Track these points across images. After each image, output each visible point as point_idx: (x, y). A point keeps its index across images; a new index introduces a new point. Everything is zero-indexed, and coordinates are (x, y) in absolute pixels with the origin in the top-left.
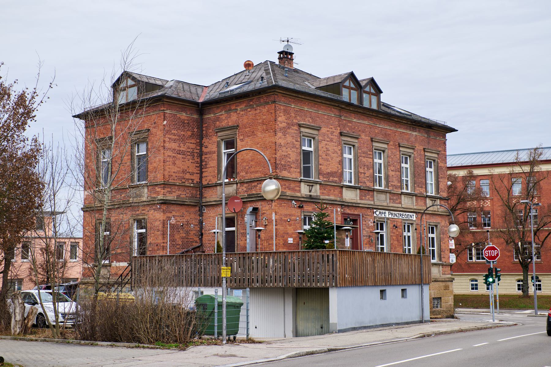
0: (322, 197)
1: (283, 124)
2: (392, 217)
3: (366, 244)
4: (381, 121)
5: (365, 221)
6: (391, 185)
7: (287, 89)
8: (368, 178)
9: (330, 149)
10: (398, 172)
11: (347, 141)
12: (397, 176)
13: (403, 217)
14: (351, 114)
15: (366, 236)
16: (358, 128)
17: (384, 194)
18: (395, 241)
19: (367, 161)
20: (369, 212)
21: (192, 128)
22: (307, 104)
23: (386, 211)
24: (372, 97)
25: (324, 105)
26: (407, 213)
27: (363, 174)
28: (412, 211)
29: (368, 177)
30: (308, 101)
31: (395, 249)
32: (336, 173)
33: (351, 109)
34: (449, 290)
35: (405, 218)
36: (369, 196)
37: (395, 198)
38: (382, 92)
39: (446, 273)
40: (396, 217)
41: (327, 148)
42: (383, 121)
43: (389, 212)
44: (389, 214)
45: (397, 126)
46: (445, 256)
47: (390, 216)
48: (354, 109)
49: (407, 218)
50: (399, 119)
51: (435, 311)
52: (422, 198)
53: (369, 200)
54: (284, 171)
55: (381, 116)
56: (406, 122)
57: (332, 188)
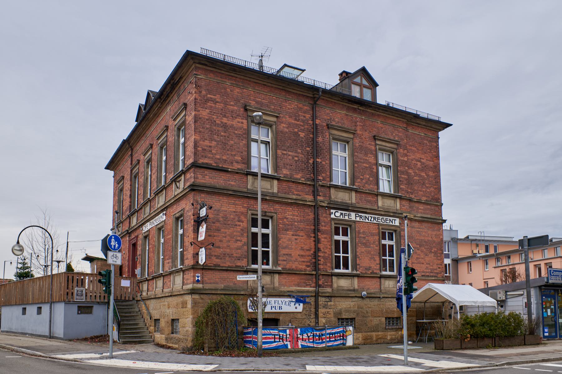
0: (357, 205)
2: (361, 220)
7: (309, 88)
13: (379, 221)
17: (348, 193)
21: (303, 146)
24: (365, 90)
26: (385, 218)
35: (381, 223)
38: (378, 85)
40: (367, 221)
43: (356, 214)
44: (356, 217)
47: (358, 219)
49: (385, 223)
51: (171, 339)
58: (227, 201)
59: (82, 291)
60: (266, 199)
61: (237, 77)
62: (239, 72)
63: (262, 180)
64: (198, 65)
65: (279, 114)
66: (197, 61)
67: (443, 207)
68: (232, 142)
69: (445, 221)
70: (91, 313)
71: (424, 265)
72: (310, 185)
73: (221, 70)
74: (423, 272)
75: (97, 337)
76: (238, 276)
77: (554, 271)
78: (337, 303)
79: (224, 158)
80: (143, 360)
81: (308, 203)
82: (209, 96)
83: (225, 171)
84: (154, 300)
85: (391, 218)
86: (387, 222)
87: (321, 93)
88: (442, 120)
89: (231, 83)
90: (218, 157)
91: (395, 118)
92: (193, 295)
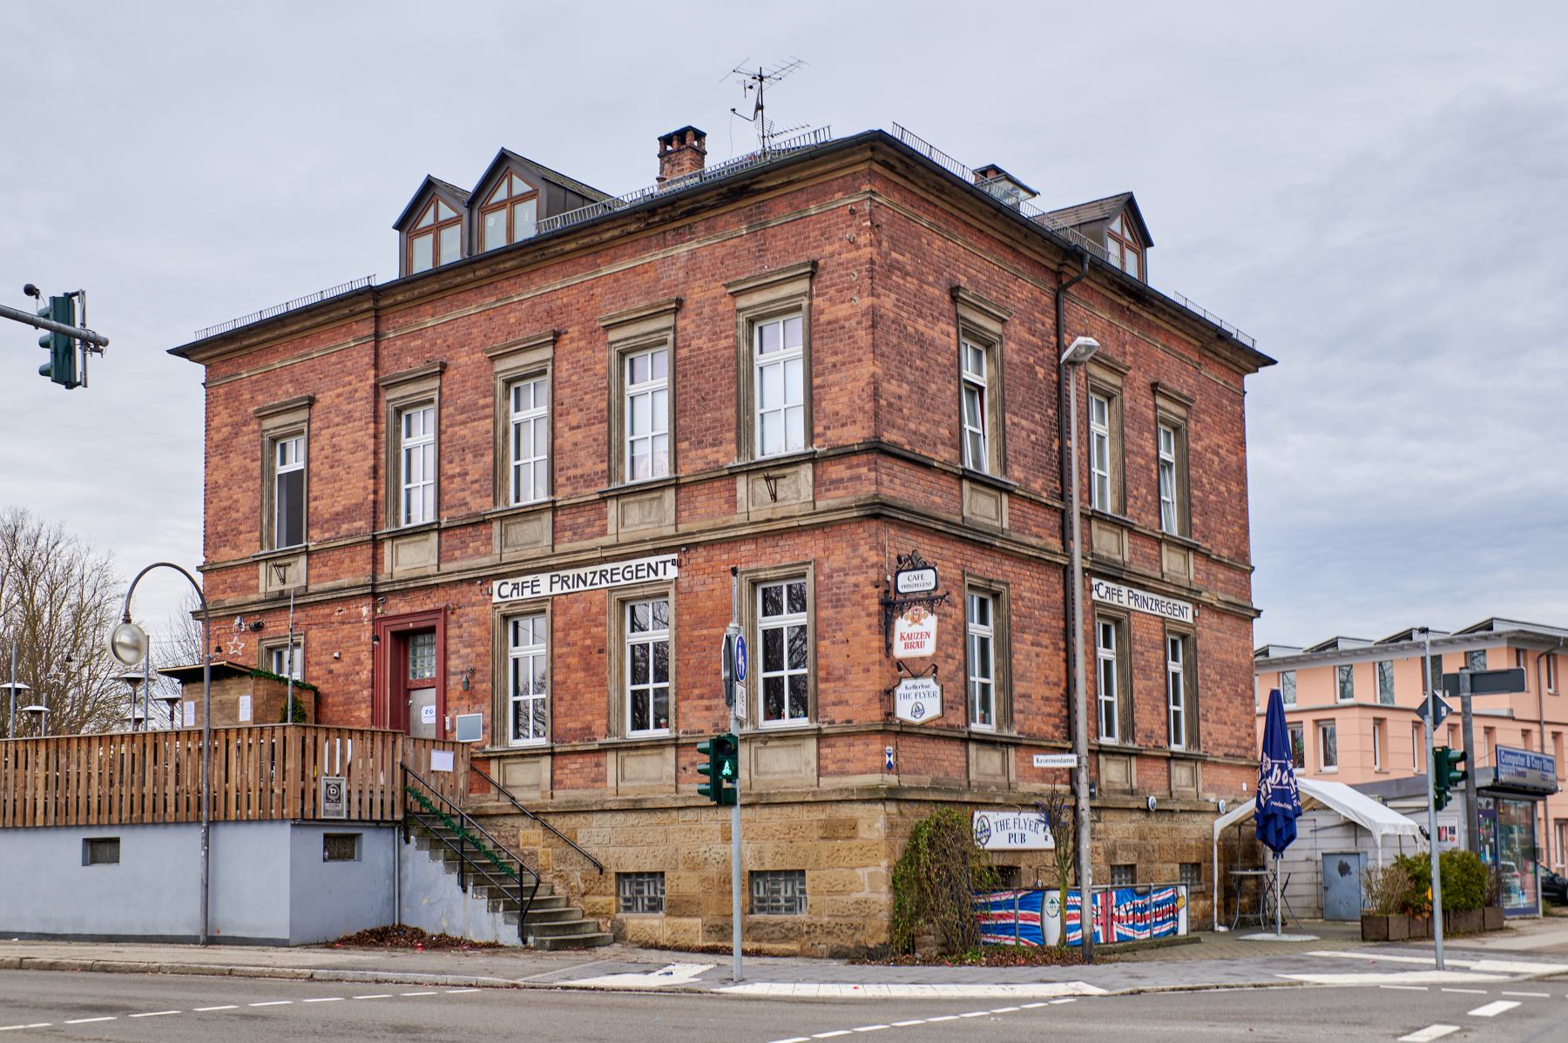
1: (224, 430)
3: (460, 698)
4: (533, 276)
5: (460, 627)
6: (568, 479)
8: (476, 486)
9: (343, 443)
10: (600, 422)
11: (402, 398)
12: (595, 440)
14: (422, 309)
15: (462, 672)
16: (445, 341)
18: (576, 670)
19: (474, 431)
20: (474, 593)
22: (281, 349)
23: (540, 576)
25: (325, 328)
26: (634, 563)
27: (458, 480)
28: (649, 547)
29: (476, 481)
30: (282, 340)
31: (574, 698)
32: (358, 506)
33: (400, 298)
34: (853, 843)
35: (623, 582)
36: (479, 543)
37: (581, 520)
39: (850, 766)
41: (334, 446)
42: (539, 273)
44: (552, 583)
45: (599, 261)
46: (846, 696)
47: (557, 589)
48: (408, 295)
49: (634, 581)
50: (583, 237)
52: (717, 484)
53: (477, 552)
54: (222, 549)
55: (508, 265)
56: (616, 232)
57: (345, 555)
58: (928, 548)
59: (339, 786)
60: (992, 545)
61: (936, 206)
62: (949, 195)
63: (972, 489)
64: (876, 167)
65: (1010, 314)
66: (880, 157)
67: (1253, 575)
68: (933, 386)
69: (1258, 613)
70: (115, 859)
71: (1226, 727)
72: (1056, 509)
73: (915, 184)
74: (1227, 746)
75: (373, 933)
76: (1035, 757)
77: (1506, 752)
78: (1109, 824)
79: (923, 430)
80: (772, 981)
81: (1058, 560)
82: (894, 255)
83: (924, 465)
84: (600, 815)
85: (653, 560)
86: (640, 574)
87: (1087, 266)
88: (1259, 348)
89: (930, 223)
90: (912, 426)
91: (1183, 336)
92: (887, 803)
